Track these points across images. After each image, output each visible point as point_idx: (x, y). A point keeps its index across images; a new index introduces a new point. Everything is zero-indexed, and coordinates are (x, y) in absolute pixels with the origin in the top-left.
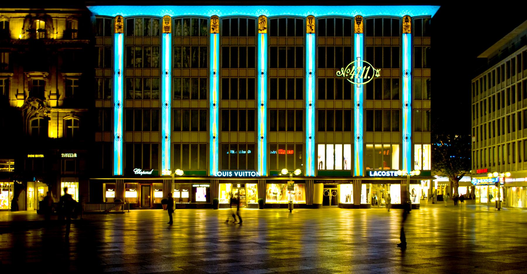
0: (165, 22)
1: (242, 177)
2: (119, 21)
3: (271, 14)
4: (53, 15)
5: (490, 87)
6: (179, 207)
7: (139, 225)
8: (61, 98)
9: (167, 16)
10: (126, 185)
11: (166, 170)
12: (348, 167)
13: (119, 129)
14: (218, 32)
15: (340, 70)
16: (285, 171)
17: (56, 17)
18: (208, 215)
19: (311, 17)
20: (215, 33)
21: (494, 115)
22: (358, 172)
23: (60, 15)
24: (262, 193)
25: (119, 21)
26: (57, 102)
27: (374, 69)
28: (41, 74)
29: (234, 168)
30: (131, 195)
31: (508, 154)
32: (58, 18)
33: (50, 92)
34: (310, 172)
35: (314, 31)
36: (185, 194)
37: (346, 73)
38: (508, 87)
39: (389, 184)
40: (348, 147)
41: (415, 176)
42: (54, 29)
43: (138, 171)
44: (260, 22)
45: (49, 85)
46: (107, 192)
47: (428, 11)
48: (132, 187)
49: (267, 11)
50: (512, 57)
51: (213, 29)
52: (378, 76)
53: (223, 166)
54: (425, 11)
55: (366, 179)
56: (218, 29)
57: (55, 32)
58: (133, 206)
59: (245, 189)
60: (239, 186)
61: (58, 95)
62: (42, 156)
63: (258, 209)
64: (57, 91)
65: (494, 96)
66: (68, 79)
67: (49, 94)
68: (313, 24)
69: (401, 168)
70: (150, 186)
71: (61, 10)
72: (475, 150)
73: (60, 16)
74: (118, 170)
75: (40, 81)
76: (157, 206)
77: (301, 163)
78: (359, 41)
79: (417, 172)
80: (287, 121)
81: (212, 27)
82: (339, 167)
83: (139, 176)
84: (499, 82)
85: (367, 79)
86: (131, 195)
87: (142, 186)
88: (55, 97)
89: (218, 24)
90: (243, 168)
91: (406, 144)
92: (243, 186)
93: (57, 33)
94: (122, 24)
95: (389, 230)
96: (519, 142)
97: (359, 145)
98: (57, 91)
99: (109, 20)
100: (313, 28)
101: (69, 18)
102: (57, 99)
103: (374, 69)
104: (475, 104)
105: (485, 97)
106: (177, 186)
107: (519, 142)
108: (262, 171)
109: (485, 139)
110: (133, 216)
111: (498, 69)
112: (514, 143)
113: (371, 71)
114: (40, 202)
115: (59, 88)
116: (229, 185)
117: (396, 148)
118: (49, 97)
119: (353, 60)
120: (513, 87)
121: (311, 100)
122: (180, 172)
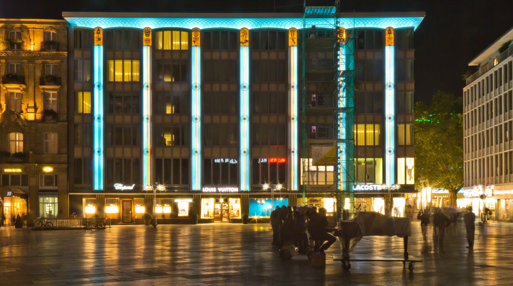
0: (146, 35)
2: (98, 33)
3: (252, 26)
4: (29, 26)
5: (480, 97)
6: (160, 222)
7: (120, 239)
8: (39, 110)
9: (147, 28)
10: (107, 200)
11: (147, 186)
13: (98, 144)
14: (199, 45)
16: (266, 187)
17: (33, 28)
18: (191, 230)
19: (293, 30)
20: (196, 46)
21: (483, 125)
23: (37, 26)
25: (98, 33)
26: (35, 116)
28: (19, 87)
29: (216, 183)
30: (112, 210)
31: (497, 166)
32: (35, 28)
33: (28, 105)
35: (296, 44)
36: (167, 210)
38: (496, 97)
39: (373, 198)
41: (396, 191)
42: (31, 40)
43: (118, 186)
44: (241, 34)
45: (27, 98)
46: (86, 207)
47: (411, 23)
48: (113, 202)
49: (248, 23)
50: (509, 61)
51: (194, 42)
53: (205, 182)
54: (408, 22)
55: (348, 192)
56: (199, 42)
57: (32, 43)
58: (113, 222)
59: (228, 204)
60: (222, 200)
61: (35, 108)
63: (242, 224)
64: (35, 104)
65: (483, 106)
66: (46, 91)
67: (26, 107)
69: (384, 181)
70: (131, 201)
71: (38, 20)
72: (467, 161)
73: (36, 27)
74: (98, 184)
75: (17, 93)
76: (138, 222)
77: (284, 178)
79: (398, 187)
80: (269, 134)
81: (193, 40)
83: (119, 191)
84: (496, 87)
86: (112, 210)
87: (123, 201)
88: (33, 110)
89: (199, 36)
90: (225, 183)
91: (390, 158)
92: (226, 201)
93: (34, 44)
94: (102, 36)
95: (373, 248)
96: (506, 154)
98: (35, 104)
99: (89, 32)
100: (296, 40)
101: (46, 29)
102: (35, 112)
104: (466, 113)
105: (475, 107)
106: (160, 201)
107: (506, 154)
108: (245, 185)
109: (476, 150)
110: (113, 232)
111: (487, 78)
112: (476, 161)
115: (36, 101)
116: (212, 200)
117: (379, 161)
118: (27, 110)
120: (501, 97)
122: (161, 188)
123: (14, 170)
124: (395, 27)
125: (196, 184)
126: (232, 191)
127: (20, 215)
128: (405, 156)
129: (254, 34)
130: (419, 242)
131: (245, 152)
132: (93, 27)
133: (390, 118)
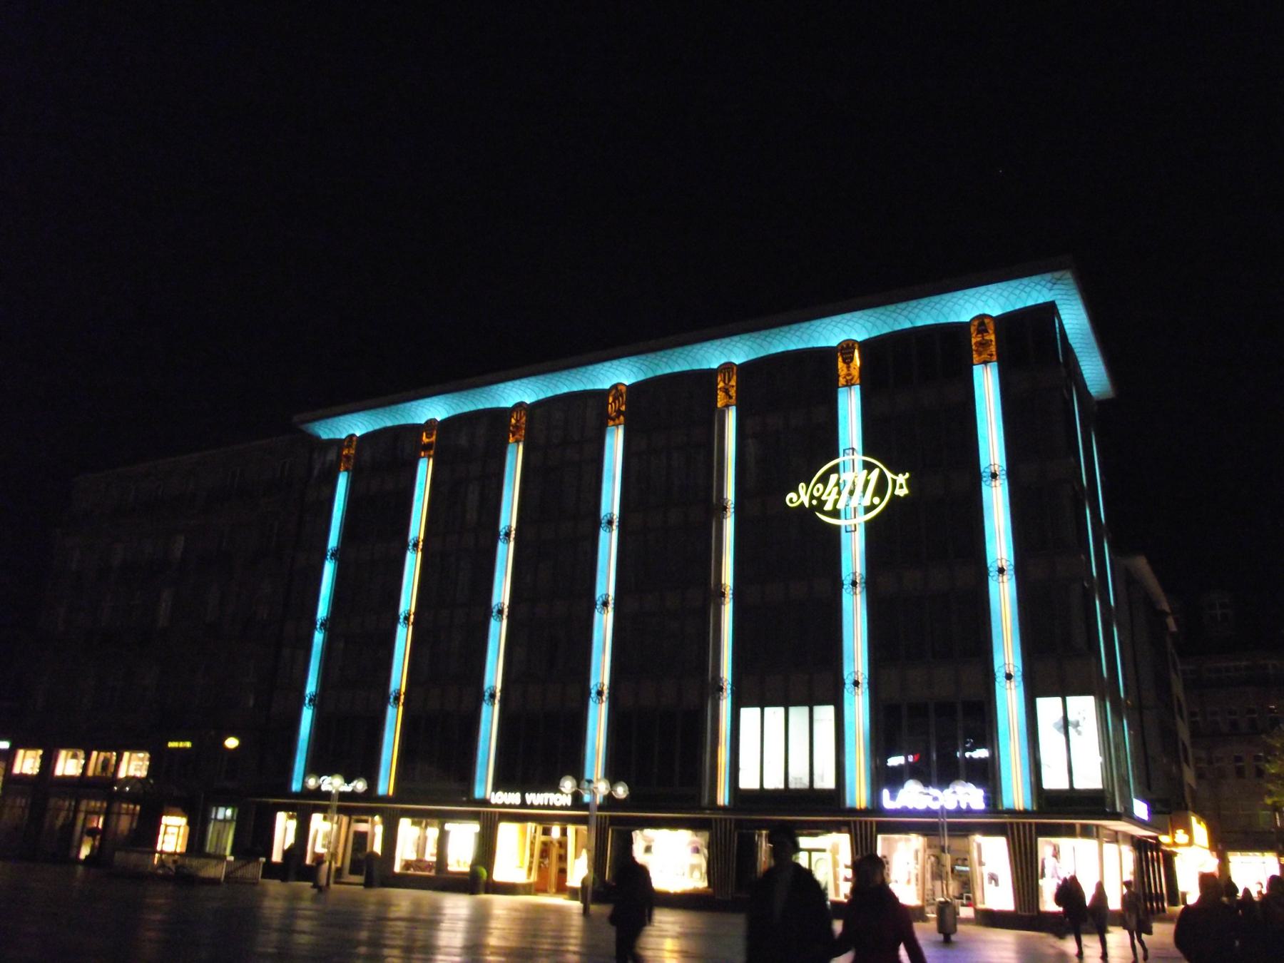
1: (539, 807)
12: (826, 781)
15: (796, 491)
22: (858, 795)
24: (1026, 871)
27: (889, 475)
34: (1016, 795)
37: (812, 497)
40: (825, 714)
52: (903, 492)
62: (188, 744)
68: (733, 383)
78: (850, 406)
82: (799, 779)
85: (873, 507)
94: (993, 337)
97: (858, 705)
100: (733, 392)
103: (889, 475)
113: (882, 480)
114: (1127, 884)
119: (837, 456)
121: (1005, 556)
123: (181, 744)
124: (996, 312)
125: (484, 786)
126: (558, 804)
127: (1255, 895)
128: (1063, 690)
129: (871, 348)
130: (396, 952)
131: (1009, 677)
132: (966, 318)
133: (1001, 571)
